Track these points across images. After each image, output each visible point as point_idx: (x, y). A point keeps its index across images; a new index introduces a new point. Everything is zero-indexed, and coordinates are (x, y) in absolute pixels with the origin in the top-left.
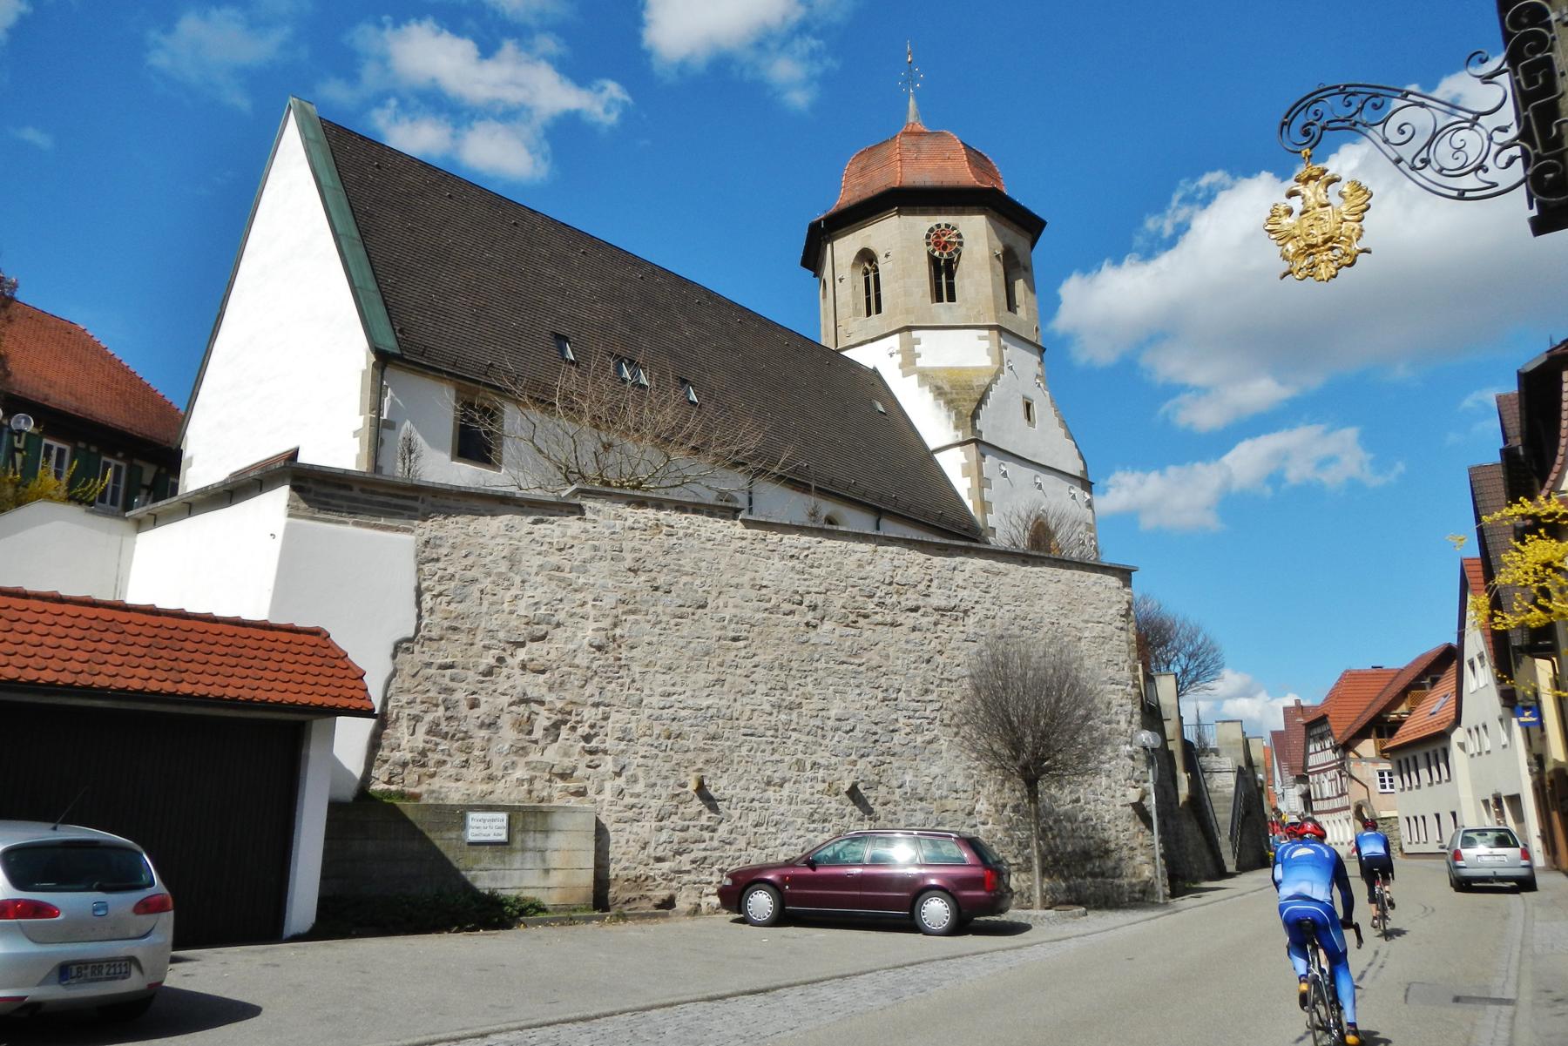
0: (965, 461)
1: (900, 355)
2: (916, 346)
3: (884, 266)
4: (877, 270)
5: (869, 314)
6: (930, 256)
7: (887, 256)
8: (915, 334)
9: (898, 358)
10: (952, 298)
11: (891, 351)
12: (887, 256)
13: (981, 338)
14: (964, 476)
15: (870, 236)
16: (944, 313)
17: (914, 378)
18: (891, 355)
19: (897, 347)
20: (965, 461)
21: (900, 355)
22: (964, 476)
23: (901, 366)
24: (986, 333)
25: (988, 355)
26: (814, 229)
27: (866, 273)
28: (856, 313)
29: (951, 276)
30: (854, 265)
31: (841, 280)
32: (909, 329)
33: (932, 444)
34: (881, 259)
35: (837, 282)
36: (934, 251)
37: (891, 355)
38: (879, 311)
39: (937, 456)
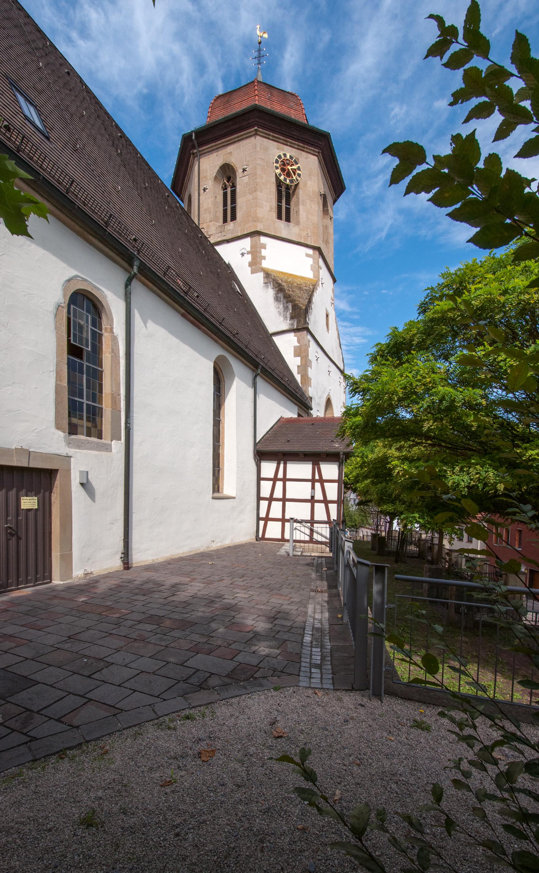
0: (298, 345)
1: (250, 256)
2: (263, 250)
3: (241, 182)
4: (234, 186)
5: (225, 221)
6: (277, 178)
7: (244, 170)
8: (263, 240)
9: (248, 258)
10: (288, 220)
11: (243, 251)
12: (244, 170)
13: (308, 255)
14: (452, 95)
15: (231, 153)
16: (282, 229)
17: (260, 276)
18: (243, 254)
19: (249, 249)
20: (298, 345)
21: (250, 256)
22: (452, 95)
23: (251, 265)
24: (310, 252)
25: (312, 269)
26: (187, 139)
27: (225, 188)
28: (216, 219)
29: (288, 202)
30: (216, 178)
31: (205, 190)
32: (259, 233)
33: (271, 329)
34: (239, 172)
35: (202, 191)
36: (280, 175)
37: (243, 254)
38: (234, 218)
39: (276, 339)
